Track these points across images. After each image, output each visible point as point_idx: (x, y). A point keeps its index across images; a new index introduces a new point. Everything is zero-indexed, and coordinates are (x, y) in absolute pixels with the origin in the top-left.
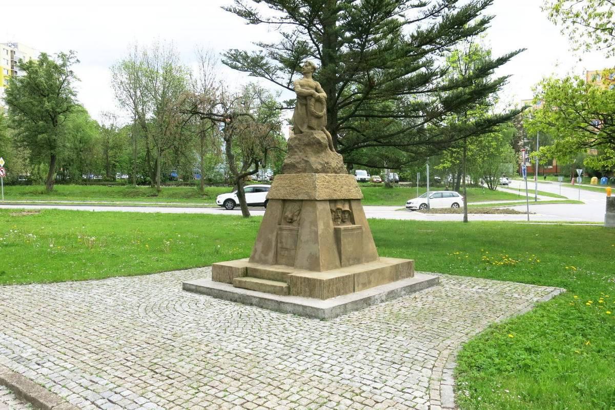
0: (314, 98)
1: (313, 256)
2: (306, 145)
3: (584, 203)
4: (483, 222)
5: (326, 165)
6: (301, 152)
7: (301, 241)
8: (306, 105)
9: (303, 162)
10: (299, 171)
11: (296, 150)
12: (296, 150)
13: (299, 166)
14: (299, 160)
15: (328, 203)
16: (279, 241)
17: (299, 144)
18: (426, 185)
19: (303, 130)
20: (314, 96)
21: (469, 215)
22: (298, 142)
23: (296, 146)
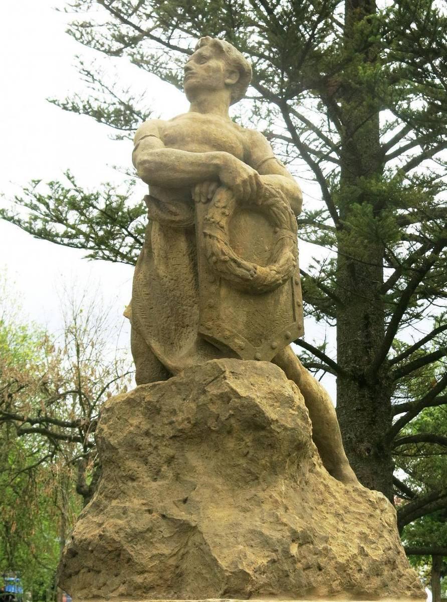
2: (181, 438)
5: (294, 550)
6: (157, 475)
8: (190, 232)
10: (138, 587)
12: (132, 465)
13: (142, 554)
17: (147, 434)
19: (170, 362)
20: (225, 177)
22: (145, 426)
23: (135, 448)
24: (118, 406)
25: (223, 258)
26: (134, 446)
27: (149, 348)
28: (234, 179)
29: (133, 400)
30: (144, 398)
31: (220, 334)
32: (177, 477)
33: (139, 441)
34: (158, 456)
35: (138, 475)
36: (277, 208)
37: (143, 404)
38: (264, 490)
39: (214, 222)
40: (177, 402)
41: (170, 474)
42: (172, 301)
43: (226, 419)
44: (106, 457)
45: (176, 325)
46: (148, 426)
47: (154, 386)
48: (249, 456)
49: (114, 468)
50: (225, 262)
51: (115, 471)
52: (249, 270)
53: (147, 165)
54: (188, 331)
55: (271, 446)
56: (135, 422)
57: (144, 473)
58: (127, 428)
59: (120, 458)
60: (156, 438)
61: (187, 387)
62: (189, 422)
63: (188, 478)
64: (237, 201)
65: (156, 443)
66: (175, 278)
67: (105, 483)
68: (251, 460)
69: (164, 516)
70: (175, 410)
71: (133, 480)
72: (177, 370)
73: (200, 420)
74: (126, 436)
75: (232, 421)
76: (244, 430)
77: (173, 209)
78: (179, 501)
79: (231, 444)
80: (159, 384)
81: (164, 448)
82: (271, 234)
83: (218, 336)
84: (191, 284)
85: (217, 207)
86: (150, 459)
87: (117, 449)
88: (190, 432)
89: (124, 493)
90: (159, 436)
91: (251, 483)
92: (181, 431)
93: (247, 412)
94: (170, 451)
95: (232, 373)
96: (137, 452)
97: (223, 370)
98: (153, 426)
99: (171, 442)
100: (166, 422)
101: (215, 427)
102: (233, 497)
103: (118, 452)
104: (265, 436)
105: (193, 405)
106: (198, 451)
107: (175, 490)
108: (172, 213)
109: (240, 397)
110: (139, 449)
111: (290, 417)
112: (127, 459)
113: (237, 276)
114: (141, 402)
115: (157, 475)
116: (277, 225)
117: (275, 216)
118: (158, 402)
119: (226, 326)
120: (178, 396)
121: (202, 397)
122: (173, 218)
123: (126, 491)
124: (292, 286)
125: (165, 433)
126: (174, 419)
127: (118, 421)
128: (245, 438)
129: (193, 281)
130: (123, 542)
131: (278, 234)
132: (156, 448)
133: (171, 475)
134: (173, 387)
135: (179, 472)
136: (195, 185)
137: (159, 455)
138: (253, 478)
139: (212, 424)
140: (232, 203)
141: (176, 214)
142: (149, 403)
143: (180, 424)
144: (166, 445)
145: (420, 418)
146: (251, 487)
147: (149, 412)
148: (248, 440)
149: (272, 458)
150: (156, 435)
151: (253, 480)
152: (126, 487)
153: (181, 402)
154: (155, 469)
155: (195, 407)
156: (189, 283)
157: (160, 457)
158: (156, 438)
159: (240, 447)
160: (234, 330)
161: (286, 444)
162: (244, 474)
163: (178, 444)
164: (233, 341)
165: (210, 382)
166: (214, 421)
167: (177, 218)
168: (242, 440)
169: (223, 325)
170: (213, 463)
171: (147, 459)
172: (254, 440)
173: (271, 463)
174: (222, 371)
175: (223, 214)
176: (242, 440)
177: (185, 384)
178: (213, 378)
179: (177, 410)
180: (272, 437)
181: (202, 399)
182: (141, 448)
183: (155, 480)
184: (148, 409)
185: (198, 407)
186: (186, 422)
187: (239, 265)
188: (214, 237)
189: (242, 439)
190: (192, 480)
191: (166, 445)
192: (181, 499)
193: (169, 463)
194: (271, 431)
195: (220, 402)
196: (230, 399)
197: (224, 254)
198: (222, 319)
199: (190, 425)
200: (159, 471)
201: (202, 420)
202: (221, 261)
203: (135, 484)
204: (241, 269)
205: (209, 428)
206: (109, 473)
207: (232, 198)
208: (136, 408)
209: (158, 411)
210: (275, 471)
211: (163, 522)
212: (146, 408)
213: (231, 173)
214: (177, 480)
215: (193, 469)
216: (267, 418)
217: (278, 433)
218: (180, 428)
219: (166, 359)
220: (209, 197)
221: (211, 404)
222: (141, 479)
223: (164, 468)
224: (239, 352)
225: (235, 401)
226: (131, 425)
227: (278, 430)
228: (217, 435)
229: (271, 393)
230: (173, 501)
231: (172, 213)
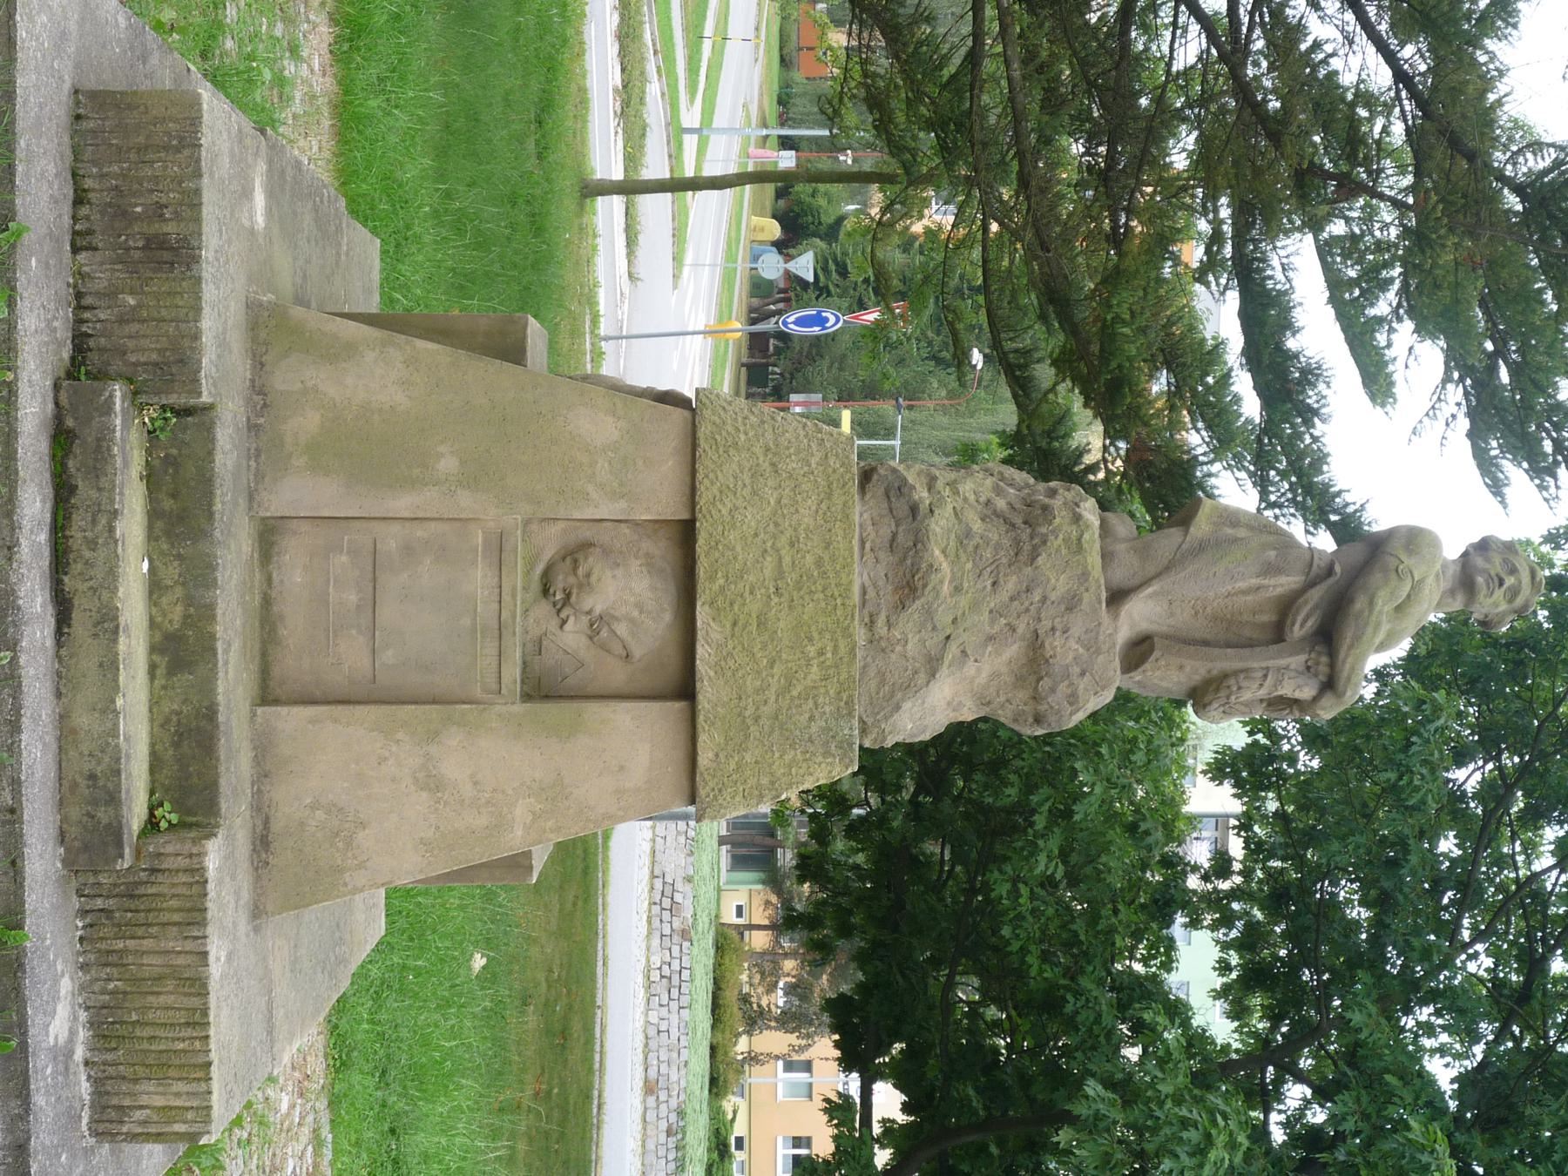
0: (1315, 699)
1: (349, 844)
2: (1035, 644)
3: (675, 287)
4: (583, 103)
7: (433, 736)
8: (1278, 633)
9: (933, 641)
11: (1011, 584)
12: (1011, 584)
13: (908, 623)
14: (943, 618)
15: (685, 516)
16: (421, 532)
18: (794, 1147)
21: (618, 202)
22: (1053, 596)
32: (991, 638)
53: (1366, 613)
60: (1039, 610)
63: (989, 648)
69: (948, 638)
71: (994, 584)
75: (1046, 707)
77: (1309, 623)
79: (1022, 695)
83: (1147, 666)
92: (1043, 643)
94: (1021, 628)
109: (1071, 715)
130: (923, 600)
139: (1045, 684)
141: (1302, 626)
142: (1080, 600)
143: (1051, 644)
145: (1021, 900)
158: (1039, 610)
167: (1297, 626)
183: (991, 612)
195: (1069, 691)
196: (1071, 704)
203: (989, 587)
205: (1042, 678)
211: (942, 637)
215: (998, 653)
223: (1003, 621)
231: (1305, 621)
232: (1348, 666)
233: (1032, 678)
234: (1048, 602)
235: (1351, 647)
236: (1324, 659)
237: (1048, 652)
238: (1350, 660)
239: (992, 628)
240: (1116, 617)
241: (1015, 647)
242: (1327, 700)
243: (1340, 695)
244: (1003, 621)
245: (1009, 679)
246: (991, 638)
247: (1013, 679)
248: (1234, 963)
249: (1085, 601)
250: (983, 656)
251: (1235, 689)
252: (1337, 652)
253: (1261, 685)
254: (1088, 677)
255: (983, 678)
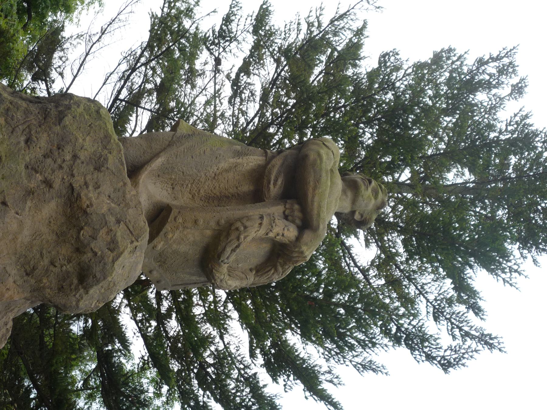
17: (75, 157)
19: (144, 177)
22: (83, 155)
24: (103, 126)
25: (242, 237)
26: (62, 143)
27: (157, 155)
28: (306, 244)
29: (109, 142)
30: (110, 153)
31: (170, 229)
32: (30, 193)
33: (68, 149)
34: (52, 169)
35: (31, 147)
36: (273, 274)
37: (106, 152)
38: (14, 282)
39: (272, 227)
40: (107, 188)
41: (32, 185)
42: (197, 175)
43: (91, 249)
44: (51, 110)
45: (175, 179)
46: (82, 158)
47: (122, 164)
48: (51, 268)
49: (39, 119)
50: (238, 238)
51: (36, 120)
52: (228, 258)
53: (319, 161)
54: (169, 189)
55: (61, 289)
56: (88, 143)
57: (34, 154)
58: (81, 135)
59: (50, 128)
60: (71, 168)
61: (121, 199)
62: (88, 207)
63: (29, 204)
64: (285, 244)
65: (66, 167)
66: (216, 178)
67: (23, 108)
68: (47, 270)
70: (99, 187)
71: (27, 141)
72: (136, 185)
73: (90, 217)
74: (72, 134)
76: (79, 264)
77: (280, 182)
78: (5, 198)
79: (65, 251)
80: (124, 169)
81: (60, 176)
82: (250, 267)
83: (168, 227)
84: (210, 192)
85: (284, 229)
86: (49, 161)
87: (59, 125)
88: (78, 206)
89: (12, 132)
90: (72, 171)
91: (23, 270)
92: (79, 195)
93: (98, 269)
94: (57, 184)
95: (136, 247)
96: (56, 145)
97: (139, 239)
98: (83, 163)
99: (67, 184)
100: (87, 179)
101: (83, 235)
102: (8, 254)
103: (56, 125)
104: (72, 284)
105: (105, 209)
106: (57, 212)
107: (16, 190)
108: (276, 180)
109: (113, 262)
110: (59, 149)
111: (89, 302)
112: (49, 135)
113: (224, 249)
114: (107, 149)
115: (32, 168)
116: (257, 271)
117: (266, 270)
118: (107, 168)
119: (177, 234)
120: (112, 190)
121: (113, 219)
122: (272, 182)
123: (15, 134)
124: (203, 282)
125: (76, 178)
126: (91, 188)
127: (88, 125)
128: (71, 264)
129: (213, 195)
131: (250, 273)
132: (61, 167)
133: (32, 186)
134: (121, 183)
135: (35, 194)
136: (300, 204)
137: (53, 171)
138: (28, 271)
139: (86, 233)
140: (285, 240)
141: (275, 184)
142: (106, 159)
143: (86, 195)
144: (63, 179)
146: (18, 270)
147: (96, 159)
148: (68, 267)
149: (48, 288)
150: (74, 167)
151: (26, 271)
152: (19, 133)
153: (107, 194)
154: (38, 167)
155: (103, 211)
156: (211, 190)
157: (51, 172)
158: (71, 168)
159: (61, 260)
160: (172, 241)
161: (63, 301)
162: (32, 263)
163: (64, 192)
164: (162, 241)
165: (128, 228)
166: (90, 234)
167: (272, 186)
168: (69, 261)
169: (178, 232)
170: (44, 229)
171: (48, 157)
172: (68, 272)
173: (44, 288)
174: (138, 238)
175: (278, 235)
176: (69, 261)
177: (124, 197)
178: (131, 229)
179: (100, 190)
180: (71, 290)
181: (112, 219)
182: (60, 151)
183: (27, 167)
184: (99, 158)
185: (104, 215)
186: (88, 203)
187: (233, 250)
188: (260, 227)
189: (70, 262)
190: (27, 209)
191: (63, 179)
192: (7, 199)
193: (44, 182)
194: (77, 289)
195: (109, 239)
196: (112, 250)
197: (245, 238)
198: (183, 230)
199: (85, 206)
200: (37, 172)
201: (90, 221)
202: (240, 234)
203: (22, 144)
204: (230, 252)
205: (82, 228)
206: (34, 113)
207: (289, 241)
208: (100, 144)
209: (98, 169)
210: (34, 291)
212: (101, 156)
213: (311, 241)
214: (26, 191)
216: (92, 286)
217: (75, 295)
218: (82, 195)
219: (146, 173)
220: (290, 218)
221: (106, 230)
222: (27, 151)
223: (39, 177)
224: (152, 245)
225: (110, 256)
226: (84, 140)
227: (77, 296)
228: (75, 237)
229: (114, 284)
230: (3, 191)
231: (276, 180)
232: (316, 204)
233: (73, 232)
234: (78, 161)
235: (315, 189)
236: (296, 207)
237: (85, 202)
238: (316, 199)
239: (29, 181)
240: (135, 184)
241: (53, 205)
242: (307, 236)
243: (315, 229)
244: (39, 177)
245: (51, 238)
246: (30, 193)
247: (54, 237)
248: (501, 136)
249: (110, 161)
250: (24, 209)
251: (242, 228)
252: (305, 195)
253: (261, 224)
254: (122, 225)
255: (25, 236)
